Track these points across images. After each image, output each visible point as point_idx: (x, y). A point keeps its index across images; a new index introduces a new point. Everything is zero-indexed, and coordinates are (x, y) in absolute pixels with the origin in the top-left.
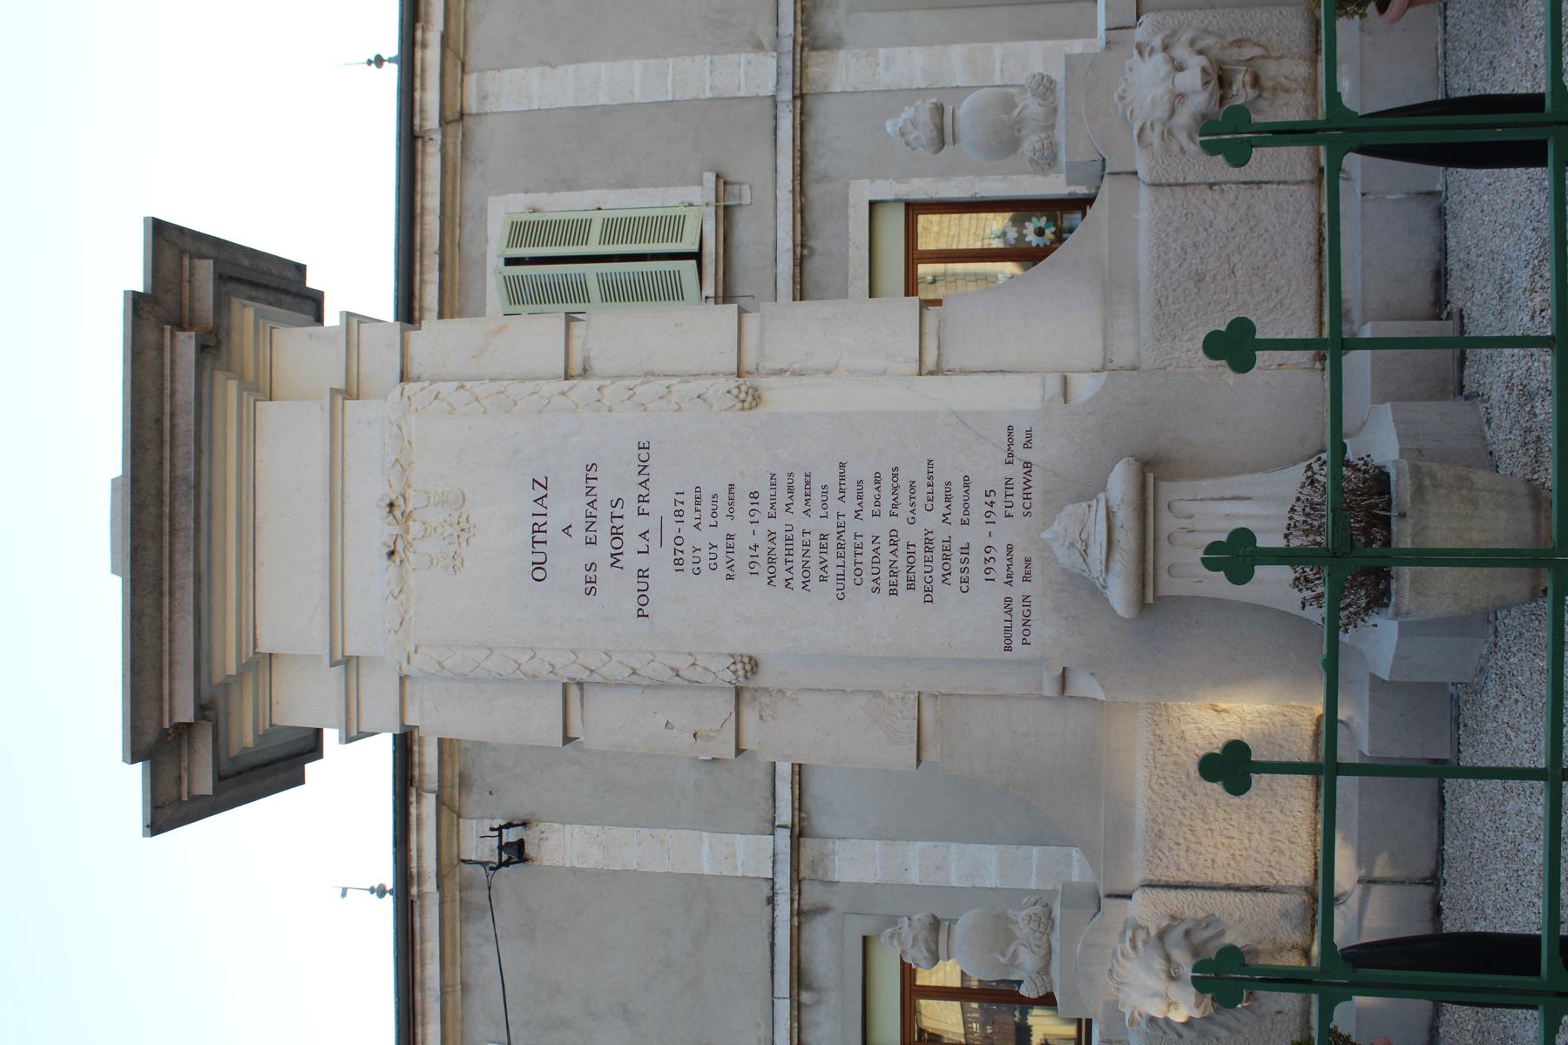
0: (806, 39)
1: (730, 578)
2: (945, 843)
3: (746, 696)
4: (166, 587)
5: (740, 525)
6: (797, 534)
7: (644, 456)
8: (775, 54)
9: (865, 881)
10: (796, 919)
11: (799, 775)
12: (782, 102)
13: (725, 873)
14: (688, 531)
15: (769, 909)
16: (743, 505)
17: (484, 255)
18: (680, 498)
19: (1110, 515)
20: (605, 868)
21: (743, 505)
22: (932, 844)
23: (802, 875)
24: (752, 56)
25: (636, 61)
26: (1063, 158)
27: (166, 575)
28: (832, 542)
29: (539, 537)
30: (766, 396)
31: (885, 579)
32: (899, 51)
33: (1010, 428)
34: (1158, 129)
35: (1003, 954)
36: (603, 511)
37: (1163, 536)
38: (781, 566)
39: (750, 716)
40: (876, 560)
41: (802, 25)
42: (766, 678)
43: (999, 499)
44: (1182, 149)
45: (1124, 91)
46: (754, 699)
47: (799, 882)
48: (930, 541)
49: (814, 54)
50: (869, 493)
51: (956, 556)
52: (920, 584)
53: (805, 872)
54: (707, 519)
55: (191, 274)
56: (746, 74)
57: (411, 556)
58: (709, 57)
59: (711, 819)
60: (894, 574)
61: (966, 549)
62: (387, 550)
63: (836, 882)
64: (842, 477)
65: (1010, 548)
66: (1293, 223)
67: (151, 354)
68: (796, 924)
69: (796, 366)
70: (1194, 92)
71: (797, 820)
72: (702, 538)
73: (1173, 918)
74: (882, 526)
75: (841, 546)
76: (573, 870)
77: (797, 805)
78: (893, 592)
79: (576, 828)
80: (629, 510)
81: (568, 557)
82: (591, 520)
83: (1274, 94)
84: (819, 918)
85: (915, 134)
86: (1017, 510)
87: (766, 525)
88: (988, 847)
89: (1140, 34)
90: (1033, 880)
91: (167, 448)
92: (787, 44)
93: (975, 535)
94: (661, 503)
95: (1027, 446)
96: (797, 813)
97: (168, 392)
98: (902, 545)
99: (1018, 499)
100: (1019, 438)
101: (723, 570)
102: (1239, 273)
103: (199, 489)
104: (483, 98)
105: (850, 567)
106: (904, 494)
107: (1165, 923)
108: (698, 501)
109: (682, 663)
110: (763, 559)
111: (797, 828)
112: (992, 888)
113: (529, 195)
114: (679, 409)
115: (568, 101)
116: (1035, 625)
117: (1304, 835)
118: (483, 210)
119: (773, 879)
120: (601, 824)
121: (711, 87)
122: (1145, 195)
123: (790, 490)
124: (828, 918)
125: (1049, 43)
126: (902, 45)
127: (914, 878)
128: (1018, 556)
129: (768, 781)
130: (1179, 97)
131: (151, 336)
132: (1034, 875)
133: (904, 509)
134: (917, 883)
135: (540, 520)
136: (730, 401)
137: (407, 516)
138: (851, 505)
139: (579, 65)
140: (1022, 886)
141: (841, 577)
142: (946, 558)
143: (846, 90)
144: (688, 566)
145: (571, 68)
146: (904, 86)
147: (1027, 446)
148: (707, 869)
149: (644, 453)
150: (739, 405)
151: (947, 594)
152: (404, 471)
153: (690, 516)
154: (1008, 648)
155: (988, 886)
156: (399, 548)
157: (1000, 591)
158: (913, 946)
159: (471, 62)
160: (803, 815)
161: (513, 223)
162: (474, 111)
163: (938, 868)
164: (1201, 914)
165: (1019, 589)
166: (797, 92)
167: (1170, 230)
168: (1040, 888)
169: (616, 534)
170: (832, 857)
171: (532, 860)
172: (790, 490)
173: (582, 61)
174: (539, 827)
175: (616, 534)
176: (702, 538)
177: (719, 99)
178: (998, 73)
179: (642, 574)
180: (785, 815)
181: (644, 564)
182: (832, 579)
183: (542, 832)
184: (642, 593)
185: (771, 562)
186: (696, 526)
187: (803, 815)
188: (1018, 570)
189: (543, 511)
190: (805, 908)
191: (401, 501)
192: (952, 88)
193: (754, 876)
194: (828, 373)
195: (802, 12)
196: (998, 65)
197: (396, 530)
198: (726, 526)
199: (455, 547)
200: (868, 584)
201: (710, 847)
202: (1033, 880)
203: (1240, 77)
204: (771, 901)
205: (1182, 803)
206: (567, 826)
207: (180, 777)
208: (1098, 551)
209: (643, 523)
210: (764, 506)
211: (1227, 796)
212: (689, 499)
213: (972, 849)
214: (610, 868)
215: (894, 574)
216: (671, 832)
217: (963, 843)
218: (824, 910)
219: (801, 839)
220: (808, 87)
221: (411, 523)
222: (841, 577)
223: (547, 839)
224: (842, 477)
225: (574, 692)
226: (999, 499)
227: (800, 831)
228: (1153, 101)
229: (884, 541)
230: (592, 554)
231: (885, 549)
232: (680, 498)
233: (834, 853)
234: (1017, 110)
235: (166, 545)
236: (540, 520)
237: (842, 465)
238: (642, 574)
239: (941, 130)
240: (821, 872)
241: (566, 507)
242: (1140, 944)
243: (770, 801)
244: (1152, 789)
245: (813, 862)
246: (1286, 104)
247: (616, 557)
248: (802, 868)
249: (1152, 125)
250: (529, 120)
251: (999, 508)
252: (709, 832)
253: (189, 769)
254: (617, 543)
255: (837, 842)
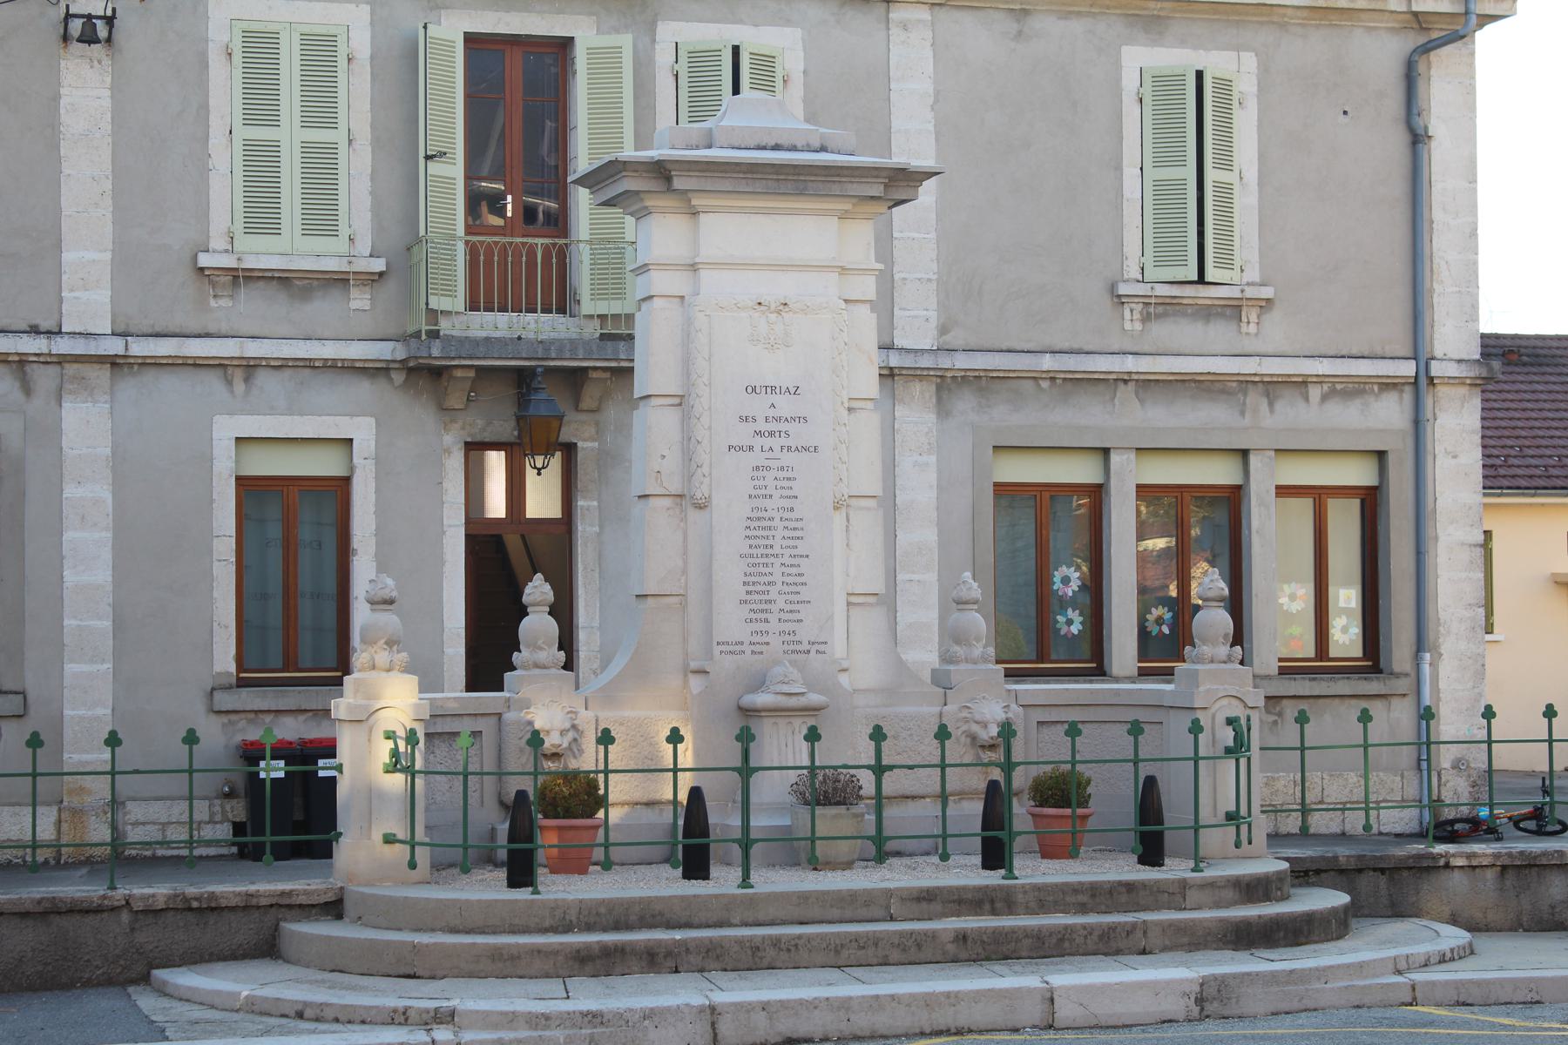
0: (949, 380)
1: (750, 496)
2: (111, 526)
3: (678, 500)
4: (749, 176)
5: (777, 502)
6: (773, 532)
7: (811, 449)
8: (935, 348)
9: (64, 437)
10: (17, 358)
11: (183, 364)
12: (888, 356)
13: (64, 277)
14: (774, 473)
15: (24, 327)
16: (787, 503)
17: (741, 22)
18: (790, 469)
19: (803, 694)
20: (61, 137)
21: (787, 503)
22: (110, 510)
23: (67, 366)
24: (934, 323)
25: (935, 199)
26: (952, 667)
27: (755, 176)
28: (769, 551)
29: (769, 390)
30: (837, 513)
31: (753, 579)
32: (932, 477)
33: (826, 643)
34: (968, 715)
35: (543, 643)
36: (783, 426)
37: (791, 720)
38: (757, 524)
39: (667, 502)
40: (760, 574)
41: (962, 377)
42: (693, 514)
43: (791, 638)
44: (958, 728)
45: (987, 699)
46: (677, 504)
47: (59, 363)
48: (770, 603)
49: (933, 387)
50: (794, 571)
51: (763, 616)
52: (749, 597)
53: (71, 369)
54: (779, 484)
55: (911, 186)
56: (916, 317)
57: (757, 314)
58: (935, 277)
59: (125, 261)
60: (754, 584)
61: (767, 621)
62: (762, 301)
63: (61, 406)
64: (802, 556)
65: (768, 644)
66: (922, 784)
67: (875, 173)
68: (10, 359)
69: (851, 528)
70: (988, 733)
71: (132, 361)
72: (770, 482)
73: (582, 732)
74: (777, 578)
75: (767, 556)
76: (56, 98)
77: (148, 361)
78: (745, 583)
79: (107, 103)
80: (784, 441)
81: (759, 406)
82: (778, 420)
83: (984, 773)
84: (17, 384)
85: (964, 590)
86: (786, 647)
87: (777, 516)
88: (110, 572)
89: (1014, 706)
90: (74, 622)
91: (823, 179)
92: (945, 362)
93: (774, 625)
94: (788, 459)
95: (818, 651)
96: (140, 361)
97: (853, 180)
98: (768, 588)
99: (792, 647)
100: (821, 648)
101: (754, 492)
102: (898, 757)
103: (801, 193)
104: (905, 27)
105: (757, 561)
106: (794, 589)
107: (580, 728)
108: (789, 479)
109: (705, 469)
110: (760, 514)
111: (122, 361)
112: (62, 578)
113: (802, 75)
114: (834, 468)
115: (896, 124)
116: (730, 657)
117: (624, 798)
118: (788, 22)
119: (60, 332)
120: (114, 133)
121: (904, 279)
122: (937, 709)
123: (795, 529)
124: (18, 395)
125: (936, 628)
126: (939, 479)
127: (70, 491)
128: (764, 648)
129: (172, 329)
130: (985, 725)
131: (884, 174)
132: (79, 623)
133: (786, 588)
134: (64, 496)
135: (778, 391)
136: (839, 496)
137: (779, 312)
138: (788, 561)
139: (934, 136)
140: (67, 610)
141: (751, 556)
142: (762, 611)
143: (896, 421)
144: (756, 474)
145: (931, 127)
146: (899, 482)
147: (818, 651)
148: (67, 257)
149: (812, 449)
150: (836, 501)
151: (744, 612)
152: (802, 310)
153: (781, 474)
154: (718, 643)
155: (65, 573)
156: (762, 308)
157: (747, 639)
158: (542, 592)
159: (942, 13)
160: (136, 367)
161: (774, 57)
162: (891, 15)
163: (83, 517)
164: (584, 747)
165: (748, 649)
166: (896, 371)
167: (919, 722)
168: (65, 630)
169: (771, 434)
170: (90, 399)
171: (66, 47)
172: (795, 529)
173: (937, 140)
174: (106, 58)
175: (771, 434)
176: (770, 482)
177: (893, 288)
178: (908, 577)
179: (751, 448)
180: (140, 348)
181: (757, 449)
182: (751, 551)
183: (100, 62)
184: (741, 448)
185: (759, 519)
186: (776, 478)
187: (136, 367)
188: (757, 648)
189: (783, 392)
190: (28, 368)
191: (787, 310)
192: (895, 531)
193: (64, 311)
194: (847, 545)
195: (975, 377)
196: (916, 577)
197: (773, 306)
198: (776, 494)
199: (763, 341)
200: (749, 570)
201: (94, 261)
202: (74, 622)
203: (994, 755)
204: (35, 330)
205: (638, 735)
206: (108, 93)
207: (637, 171)
208: (786, 689)
209: (777, 448)
210: (787, 515)
211: (755, 742)
212: (790, 475)
213: (107, 555)
214: (62, 141)
215: (754, 584)
216: (109, 216)
217: (113, 545)
218: (27, 389)
219: (109, 365)
220: (901, 382)
221: (776, 315)
222: (751, 556)
223: (92, 67)
224: (802, 556)
225: (677, 401)
226: (791, 638)
227: (118, 364)
228: (983, 713)
229: (770, 579)
230: (761, 420)
231: (767, 579)
232: (790, 469)
233: (95, 402)
234: (975, 643)
235: (770, 177)
236: (778, 391)
237: (807, 556)
238: (751, 448)
239: (966, 603)
240: (71, 387)
241: (785, 405)
242: (569, 715)
243: (150, 331)
244: (645, 719)
245: (83, 378)
246: (979, 779)
247: (759, 433)
248: (76, 366)
249: (970, 713)
250: (880, 77)
251: (787, 638)
252: (112, 259)
253: (641, 176)
254: (767, 434)
255: (108, 406)
